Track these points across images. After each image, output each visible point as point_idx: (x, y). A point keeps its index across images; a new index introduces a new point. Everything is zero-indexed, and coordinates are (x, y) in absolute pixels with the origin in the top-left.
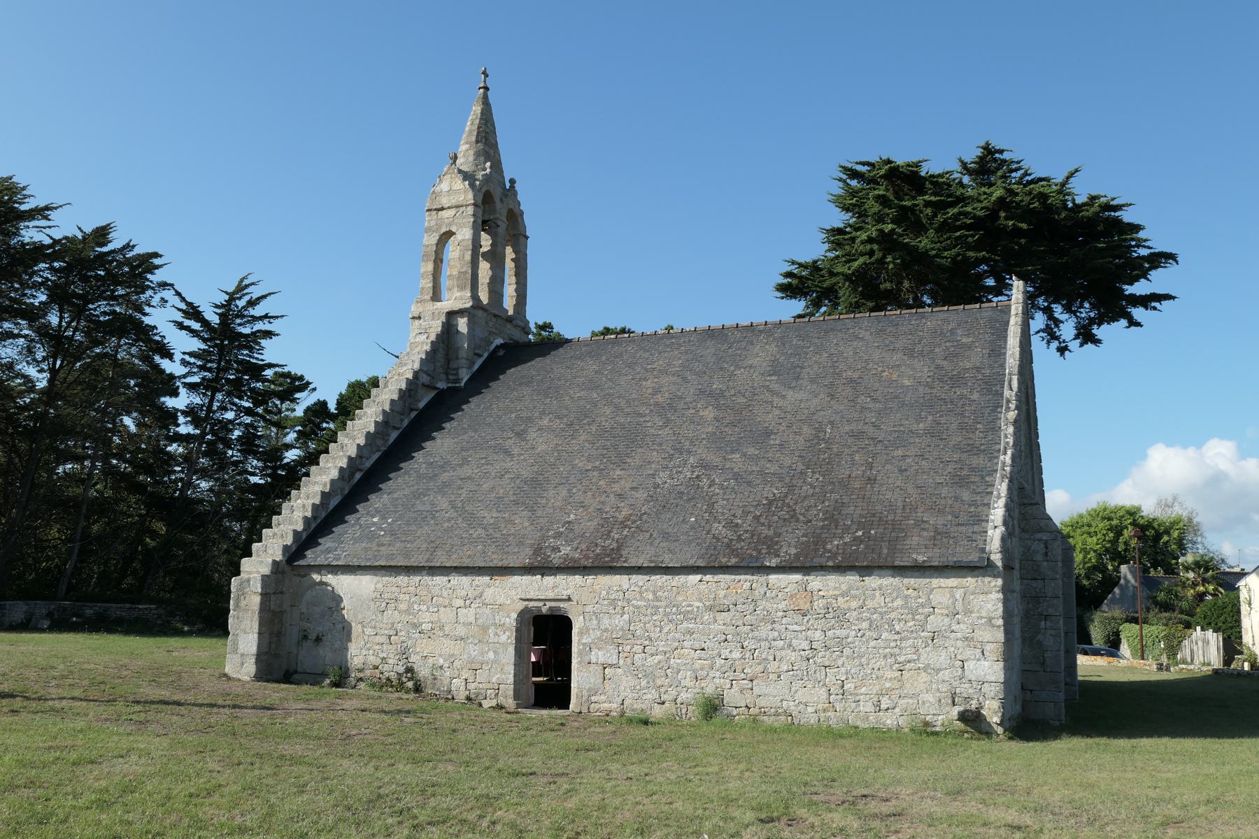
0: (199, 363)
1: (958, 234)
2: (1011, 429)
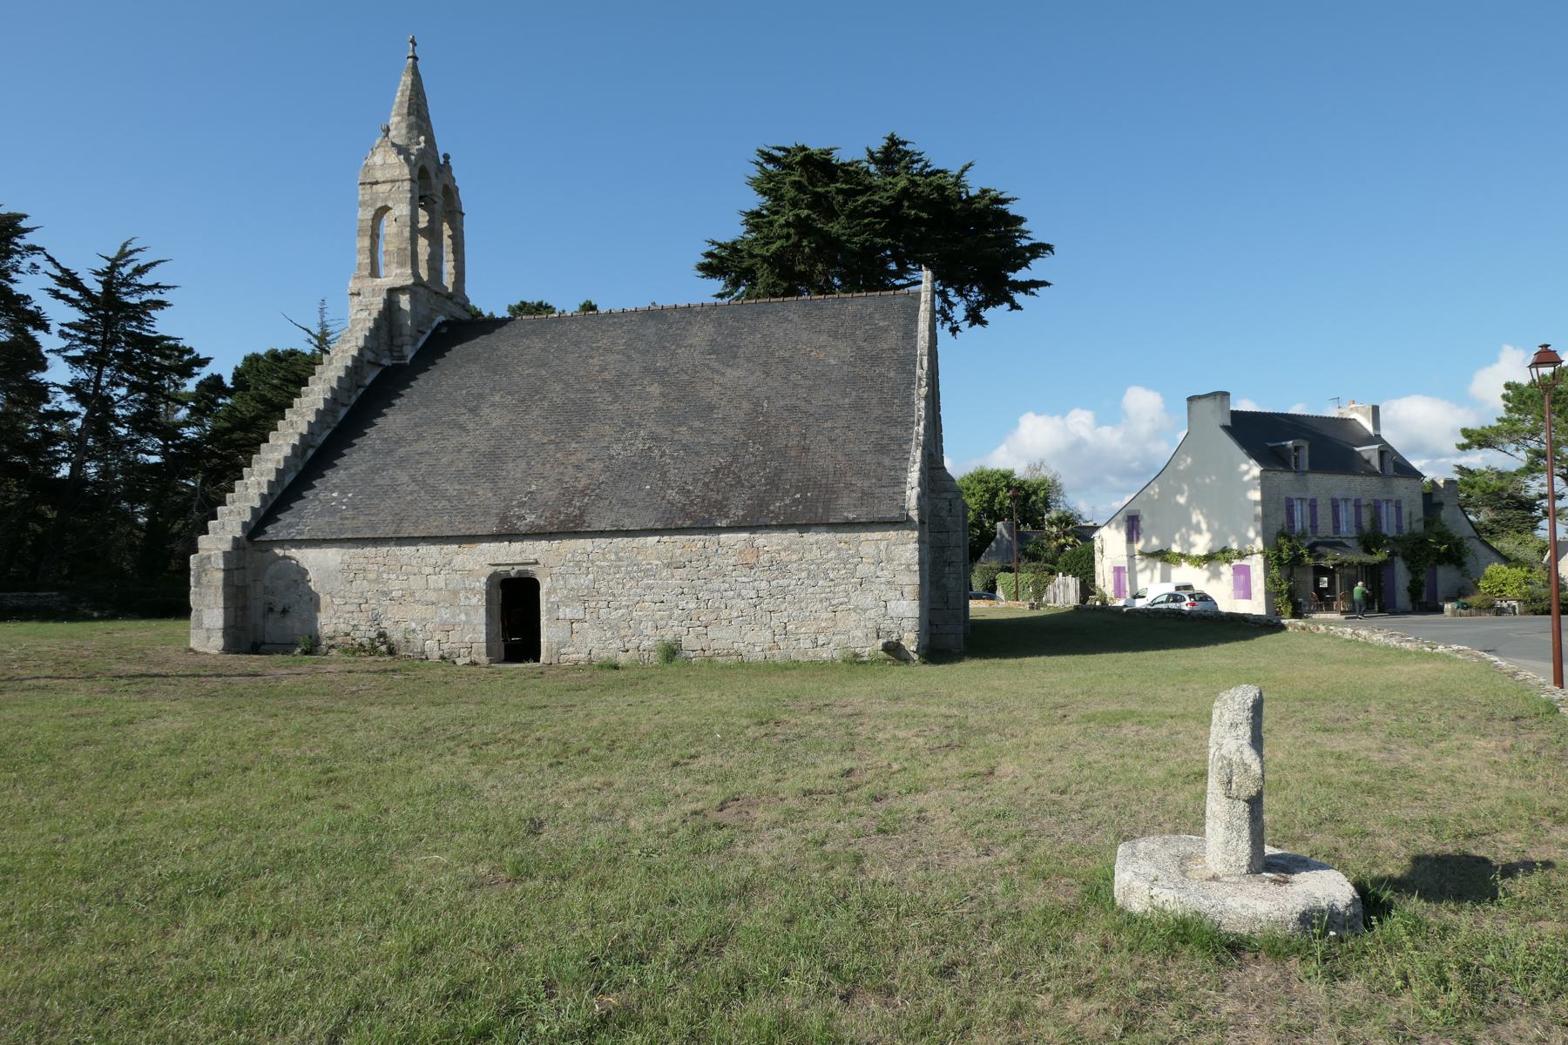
0: (82, 335)
1: (866, 221)
2: (923, 404)
